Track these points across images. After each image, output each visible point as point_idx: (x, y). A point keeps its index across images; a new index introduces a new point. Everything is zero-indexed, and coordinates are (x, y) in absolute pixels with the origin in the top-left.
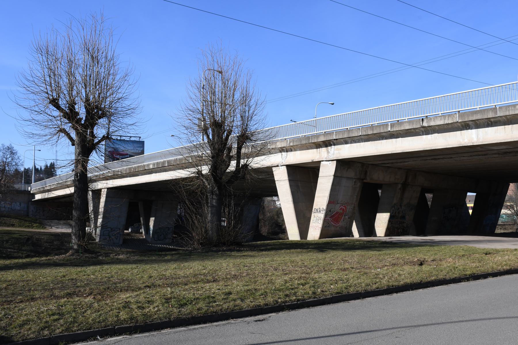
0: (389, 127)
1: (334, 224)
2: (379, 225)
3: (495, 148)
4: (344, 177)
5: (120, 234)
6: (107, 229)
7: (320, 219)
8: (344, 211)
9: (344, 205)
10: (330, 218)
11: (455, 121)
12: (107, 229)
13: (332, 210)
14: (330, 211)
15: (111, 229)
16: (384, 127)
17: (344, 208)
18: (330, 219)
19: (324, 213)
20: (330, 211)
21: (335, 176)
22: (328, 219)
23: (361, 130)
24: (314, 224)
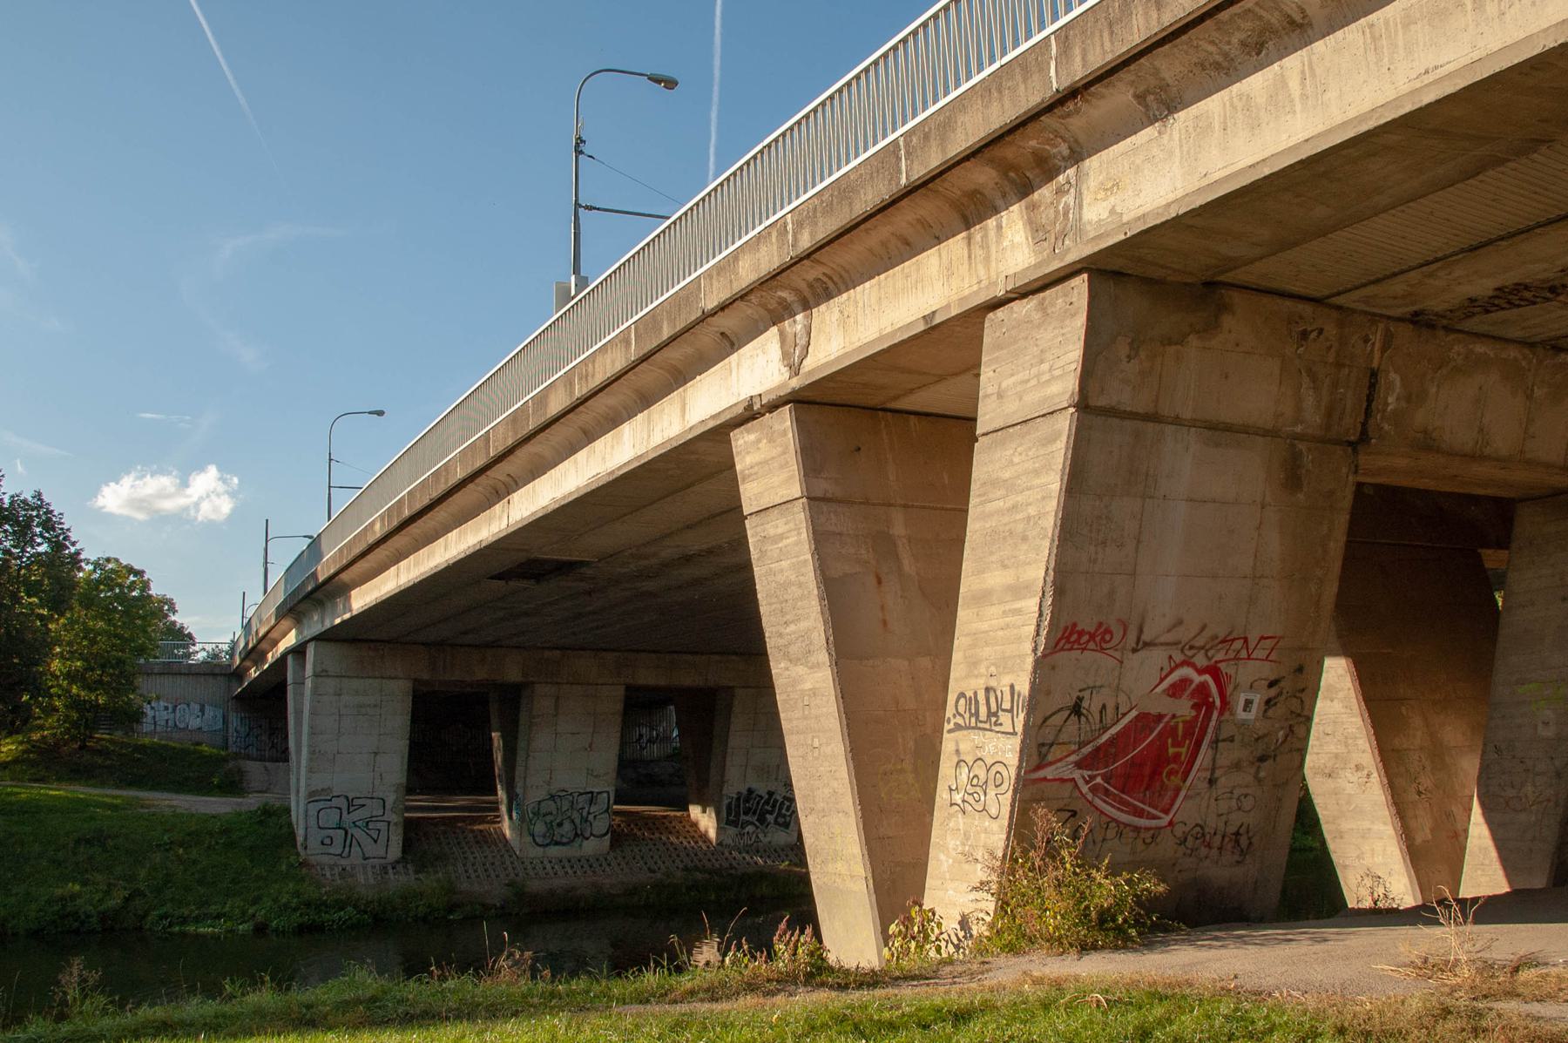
1: (1124, 818)
2: (1510, 793)
4: (1177, 421)
5: (389, 823)
6: (330, 800)
7: (327, 841)
8: (1211, 706)
9: (1200, 660)
10: (1079, 765)
12: (330, 800)
13: (1092, 705)
14: (1076, 709)
15: (350, 802)
17: (1207, 678)
18: (1086, 773)
19: (1019, 728)
20: (1076, 709)
21: (1084, 405)
22: (1062, 780)
24: (960, 815)
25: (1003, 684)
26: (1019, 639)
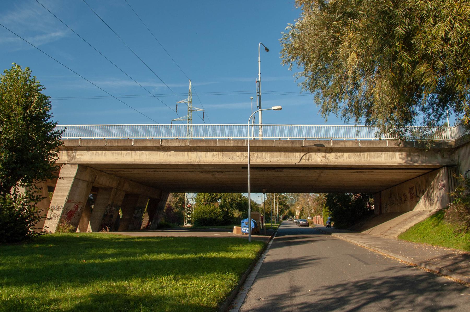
0: (133, 142)
3: (206, 168)
4: (81, 180)
9: (77, 205)
10: (66, 215)
11: (187, 145)
14: (67, 209)
16: (128, 142)
20: (67, 209)
21: (75, 178)
23: (107, 141)
25: (60, 206)
26: (63, 201)
